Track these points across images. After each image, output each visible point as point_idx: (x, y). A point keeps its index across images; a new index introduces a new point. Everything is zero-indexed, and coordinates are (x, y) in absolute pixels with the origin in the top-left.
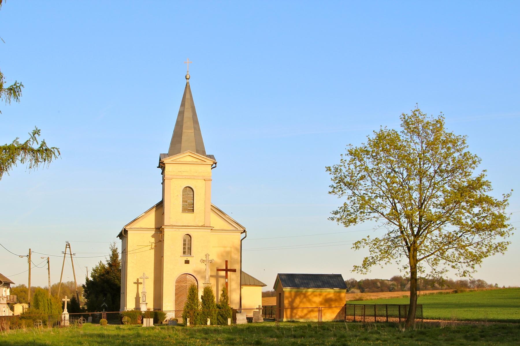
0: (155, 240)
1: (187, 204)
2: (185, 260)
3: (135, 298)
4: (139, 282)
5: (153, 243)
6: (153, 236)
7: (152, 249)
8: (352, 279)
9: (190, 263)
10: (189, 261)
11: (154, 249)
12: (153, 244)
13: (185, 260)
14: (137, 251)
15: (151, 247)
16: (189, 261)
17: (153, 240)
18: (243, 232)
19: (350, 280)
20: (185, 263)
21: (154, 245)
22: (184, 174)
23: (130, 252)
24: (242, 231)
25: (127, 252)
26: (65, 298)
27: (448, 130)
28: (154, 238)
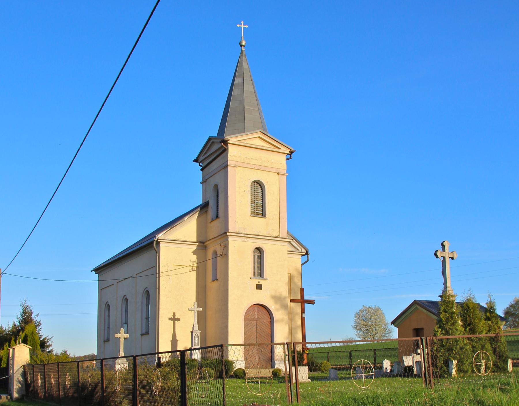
0: (197, 258)
1: (254, 205)
2: (257, 285)
3: (171, 341)
4: (176, 317)
5: (195, 262)
6: (194, 253)
7: (193, 271)
8: (92, 354)
9: (257, 290)
10: (261, 285)
11: (195, 271)
12: (194, 263)
13: (257, 285)
14: (172, 273)
15: (191, 268)
16: (261, 285)
17: (194, 258)
18: (305, 254)
19: (91, 354)
20: (257, 289)
21: (196, 265)
22: (254, 162)
23: (165, 274)
24: (304, 253)
25: (159, 273)
26: (120, 333)
27: (234, 248)
28: (196, 255)
